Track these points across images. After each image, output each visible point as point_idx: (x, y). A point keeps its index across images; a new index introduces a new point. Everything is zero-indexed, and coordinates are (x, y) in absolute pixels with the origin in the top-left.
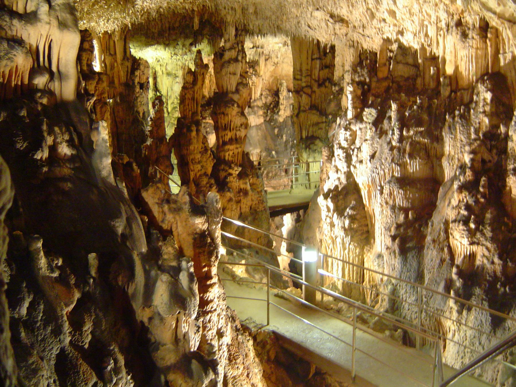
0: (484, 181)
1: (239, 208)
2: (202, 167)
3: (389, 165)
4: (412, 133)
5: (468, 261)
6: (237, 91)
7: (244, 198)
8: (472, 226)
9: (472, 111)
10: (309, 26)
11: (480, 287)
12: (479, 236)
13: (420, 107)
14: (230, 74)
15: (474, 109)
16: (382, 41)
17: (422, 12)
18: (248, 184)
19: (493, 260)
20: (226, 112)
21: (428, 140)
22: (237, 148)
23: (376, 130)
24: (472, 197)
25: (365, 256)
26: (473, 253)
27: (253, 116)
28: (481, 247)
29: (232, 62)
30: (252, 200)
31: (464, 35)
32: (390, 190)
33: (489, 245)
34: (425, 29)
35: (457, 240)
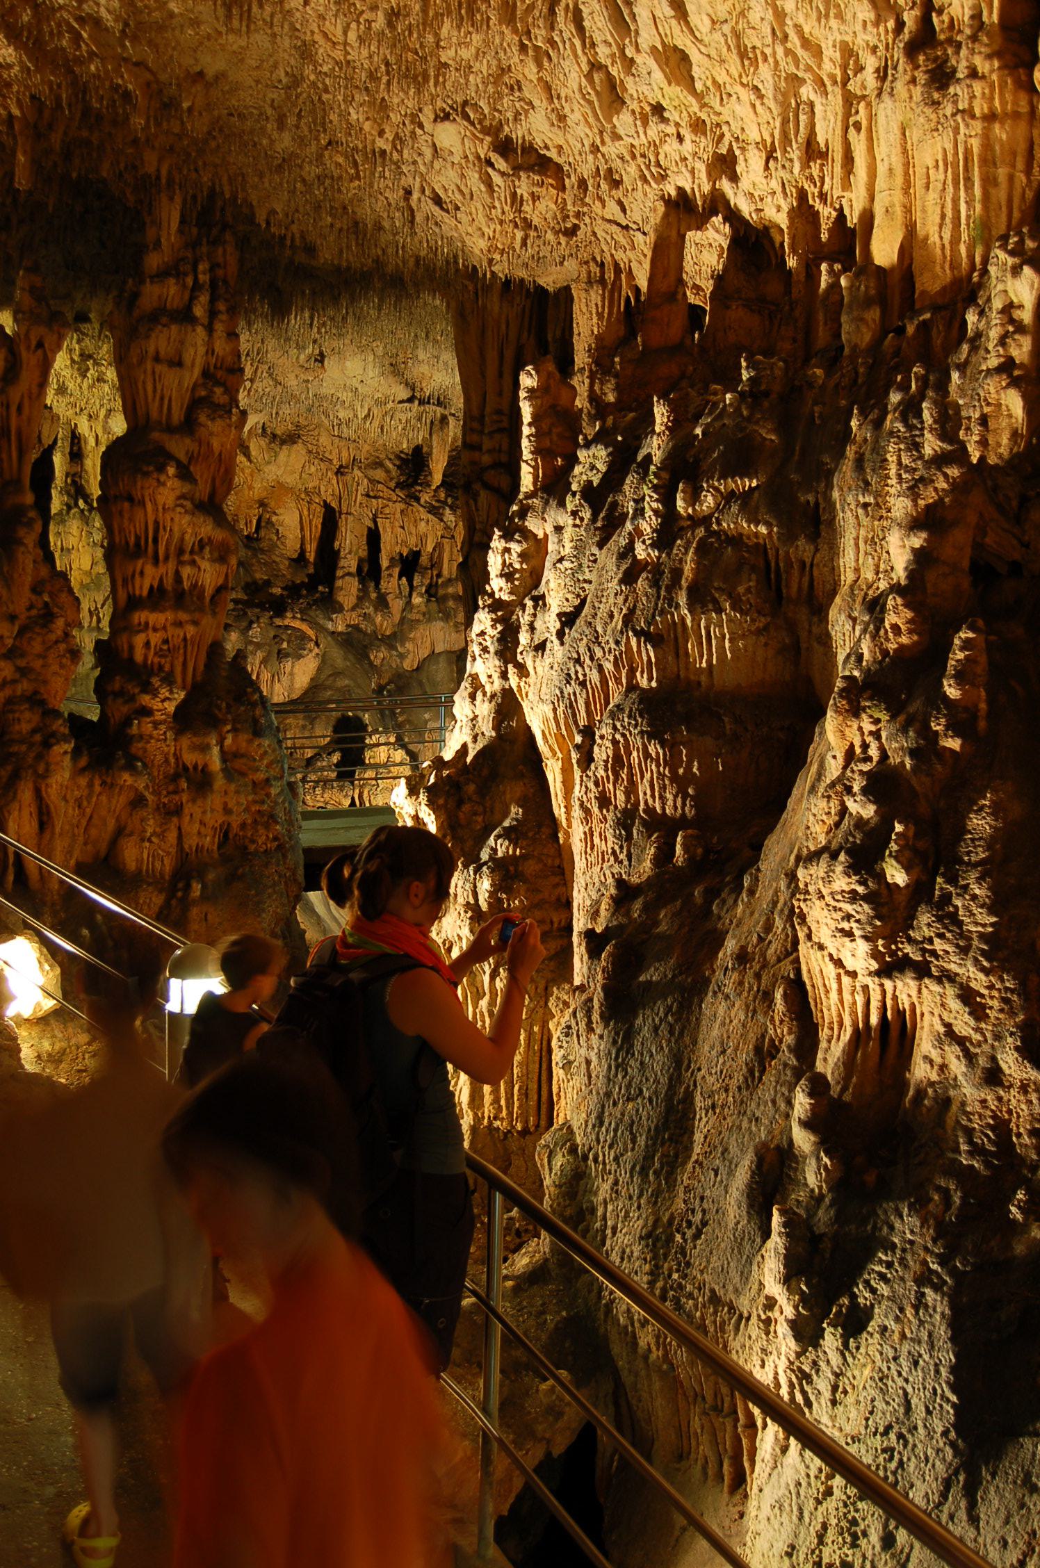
0: (966, 645)
1: (172, 836)
2: (23, 672)
3: (617, 643)
4: (709, 501)
5: (875, 1059)
6: (189, 425)
7: (194, 801)
8: (897, 876)
9: (955, 376)
10: (438, 201)
11: (920, 1206)
12: (927, 932)
13: (754, 395)
14: (157, 359)
15: (962, 368)
16: (661, 208)
17: (786, 36)
18: (216, 751)
19: (993, 1059)
20: (137, 495)
21: (769, 525)
22: (179, 624)
23: (594, 519)
24: (904, 730)
25: (552, 1025)
26: (900, 1014)
27: (440, 624)
28: (936, 988)
29: (164, 320)
30: (227, 811)
31: (941, 77)
32: (615, 742)
33: (979, 981)
34: (803, 118)
35: (821, 947)
